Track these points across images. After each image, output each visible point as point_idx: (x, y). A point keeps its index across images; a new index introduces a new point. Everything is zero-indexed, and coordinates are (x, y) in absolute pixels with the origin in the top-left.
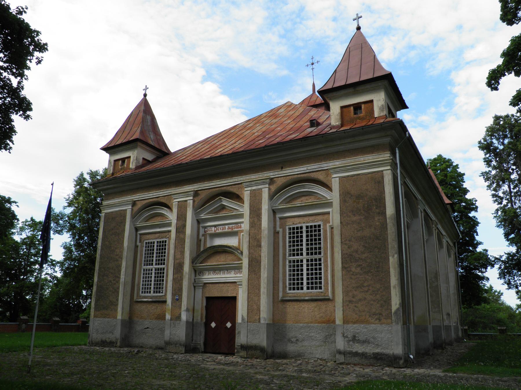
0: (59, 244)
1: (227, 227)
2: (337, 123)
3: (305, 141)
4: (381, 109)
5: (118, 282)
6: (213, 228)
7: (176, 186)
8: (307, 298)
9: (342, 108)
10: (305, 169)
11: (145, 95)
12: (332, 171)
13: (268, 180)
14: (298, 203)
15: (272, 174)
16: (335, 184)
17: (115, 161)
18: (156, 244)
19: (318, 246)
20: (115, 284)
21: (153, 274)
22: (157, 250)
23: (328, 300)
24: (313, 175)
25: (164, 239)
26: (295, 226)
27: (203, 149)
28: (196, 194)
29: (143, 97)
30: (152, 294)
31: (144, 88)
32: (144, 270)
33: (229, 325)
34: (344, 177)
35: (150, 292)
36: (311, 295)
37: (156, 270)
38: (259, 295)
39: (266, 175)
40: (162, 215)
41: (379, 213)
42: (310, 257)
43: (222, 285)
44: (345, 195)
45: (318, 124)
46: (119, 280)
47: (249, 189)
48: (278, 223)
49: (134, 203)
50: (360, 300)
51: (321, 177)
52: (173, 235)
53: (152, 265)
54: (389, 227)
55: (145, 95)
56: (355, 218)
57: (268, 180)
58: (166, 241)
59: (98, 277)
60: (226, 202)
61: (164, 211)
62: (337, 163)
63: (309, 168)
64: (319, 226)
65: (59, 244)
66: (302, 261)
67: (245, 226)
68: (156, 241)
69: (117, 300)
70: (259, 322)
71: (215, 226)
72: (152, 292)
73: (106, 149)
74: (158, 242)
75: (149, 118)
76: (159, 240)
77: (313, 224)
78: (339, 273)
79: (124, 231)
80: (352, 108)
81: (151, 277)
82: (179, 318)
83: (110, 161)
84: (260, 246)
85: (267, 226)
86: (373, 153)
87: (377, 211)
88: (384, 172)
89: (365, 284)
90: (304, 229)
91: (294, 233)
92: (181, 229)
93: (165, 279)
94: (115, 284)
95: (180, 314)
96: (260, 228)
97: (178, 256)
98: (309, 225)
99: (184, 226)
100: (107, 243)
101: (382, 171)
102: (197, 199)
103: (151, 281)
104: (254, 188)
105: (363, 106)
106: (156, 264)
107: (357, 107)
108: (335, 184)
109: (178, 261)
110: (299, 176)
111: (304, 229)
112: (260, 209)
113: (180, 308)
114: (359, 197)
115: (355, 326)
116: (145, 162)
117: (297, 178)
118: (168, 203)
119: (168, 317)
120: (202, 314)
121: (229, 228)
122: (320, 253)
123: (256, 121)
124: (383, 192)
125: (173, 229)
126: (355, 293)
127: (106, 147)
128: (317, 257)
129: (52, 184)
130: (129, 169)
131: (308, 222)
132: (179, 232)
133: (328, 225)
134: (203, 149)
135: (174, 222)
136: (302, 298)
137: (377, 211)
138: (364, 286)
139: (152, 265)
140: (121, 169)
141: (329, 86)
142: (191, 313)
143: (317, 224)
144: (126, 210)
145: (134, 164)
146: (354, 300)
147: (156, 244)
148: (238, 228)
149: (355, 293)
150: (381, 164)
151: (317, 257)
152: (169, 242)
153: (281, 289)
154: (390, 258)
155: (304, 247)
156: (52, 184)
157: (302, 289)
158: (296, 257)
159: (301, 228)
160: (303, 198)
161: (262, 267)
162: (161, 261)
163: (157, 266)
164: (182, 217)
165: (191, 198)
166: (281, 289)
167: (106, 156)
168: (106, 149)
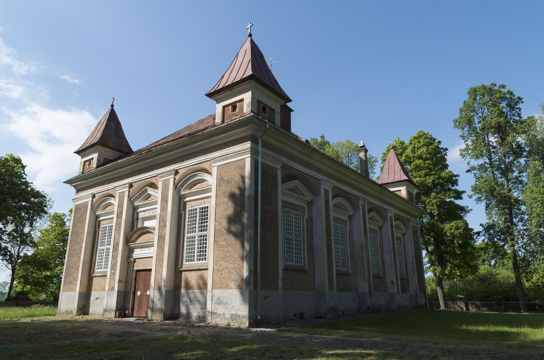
4: (248, 107)
5: (79, 261)
11: (112, 106)
12: (212, 161)
13: (173, 172)
14: (194, 189)
15: (176, 166)
16: (214, 171)
18: (198, 210)
21: (196, 241)
26: (192, 208)
28: (131, 186)
32: (187, 238)
36: (198, 265)
37: (199, 237)
38: (162, 267)
40: (203, 181)
42: (201, 233)
43: (145, 259)
44: (220, 180)
47: (162, 179)
50: (224, 269)
52: (115, 220)
54: (246, 206)
55: (112, 106)
57: (173, 172)
61: (206, 176)
71: (144, 211)
73: (78, 152)
75: (113, 125)
79: (86, 218)
82: (113, 289)
95: (114, 285)
102: (177, 177)
107: (234, 106)
108: (214, 171)
112: (167, 196)
115: (219, 291)
118: (209, 170)
119: (107, 288)
121: (152, 212)
126: (221, 262)
131: (200, 205)
139: (195, 232)
143: (206, 206)
145: (96, 164)
146: (220, 269)
149: (221, 262)
154: (245, 232)
158: (203, 232)
160: (199, 185)
162: (204, 228)
163: (201, 233)
167: (78, 160)
168: (78, 152)
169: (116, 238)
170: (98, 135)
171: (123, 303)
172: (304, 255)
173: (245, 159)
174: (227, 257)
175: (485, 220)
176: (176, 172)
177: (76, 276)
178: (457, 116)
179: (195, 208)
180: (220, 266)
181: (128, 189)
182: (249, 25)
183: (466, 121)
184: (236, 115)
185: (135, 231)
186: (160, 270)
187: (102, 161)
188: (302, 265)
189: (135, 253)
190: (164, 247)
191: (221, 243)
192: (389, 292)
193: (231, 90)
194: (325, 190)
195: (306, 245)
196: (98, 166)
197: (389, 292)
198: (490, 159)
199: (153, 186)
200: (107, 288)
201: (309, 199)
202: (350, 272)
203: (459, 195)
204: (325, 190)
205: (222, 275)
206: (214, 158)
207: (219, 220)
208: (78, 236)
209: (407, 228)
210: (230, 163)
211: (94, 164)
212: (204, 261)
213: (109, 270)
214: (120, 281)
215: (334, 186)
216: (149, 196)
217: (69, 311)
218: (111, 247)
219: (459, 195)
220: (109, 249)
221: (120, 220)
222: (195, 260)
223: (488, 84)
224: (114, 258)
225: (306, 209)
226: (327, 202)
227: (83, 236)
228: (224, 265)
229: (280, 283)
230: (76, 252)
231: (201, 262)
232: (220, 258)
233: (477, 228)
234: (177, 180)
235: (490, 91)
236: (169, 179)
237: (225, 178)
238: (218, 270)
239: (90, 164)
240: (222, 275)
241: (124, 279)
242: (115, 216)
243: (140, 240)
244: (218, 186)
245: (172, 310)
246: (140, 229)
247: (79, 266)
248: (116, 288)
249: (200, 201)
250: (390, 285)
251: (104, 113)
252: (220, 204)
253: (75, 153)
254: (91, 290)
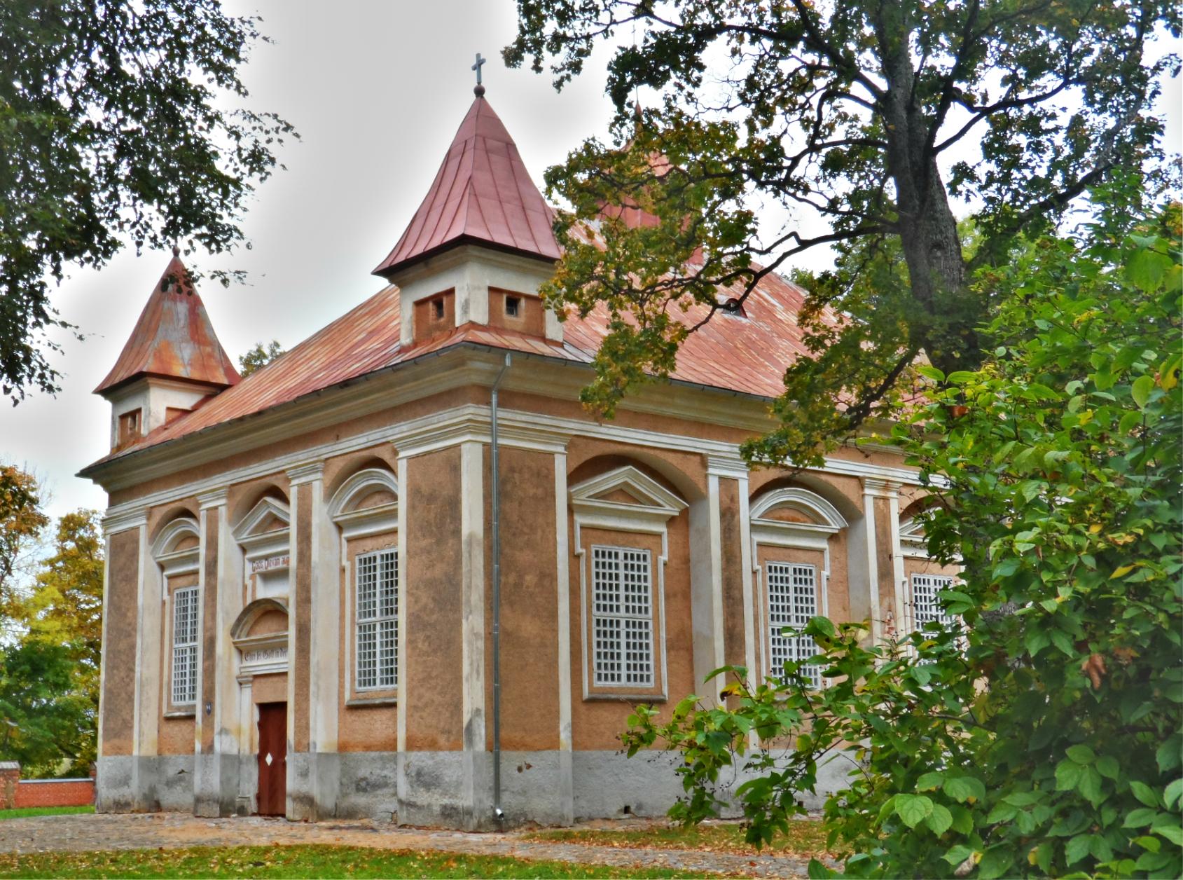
6: (264, 563)
7: (205, 477)
10: (364, 440)
11: (479, 92)
18: (378, 561)
26: (367, 556)
31: (474, 62)
34: (417, 456)
49: (149, 513)
55: (479, 92)
59: (107, 673)
62: (301, 457)
63: (371, 438)
69: (132, 717)
83: (113, 417)
86: (450, 406)
89: (434, 674)
97: (209, 624)
107: (440, 302)
113: (213, 729)
116: (176, 414)
119: (198, 747)
120: (252, 740)
127: (387, 265)
136: (613, 696)
138: (431, 678)
144: (138, 528)
149: (422, 690)
154: (464, 621)
165: (223, 501)
172: (658, 661)
173: (458, 445)
177: (128, 717)
179: (371, 554)
194: (723, 480)
195: (663, 634)
201: (671, 510)
202: (665, 690)
204: (723, 480)
210: (430, 452)
213: (198, 702)
217: (123, 800)
218: (199, 644)
220: (194, 650)
222: (378, 681)
225: (665, 539)
226: (729, 514)
228: (428, 696)
229: (565, 736)
236: (309, 483)
242: (201, 566)
247: (133, 693)
249: (381, 541)
253: (78, 475)
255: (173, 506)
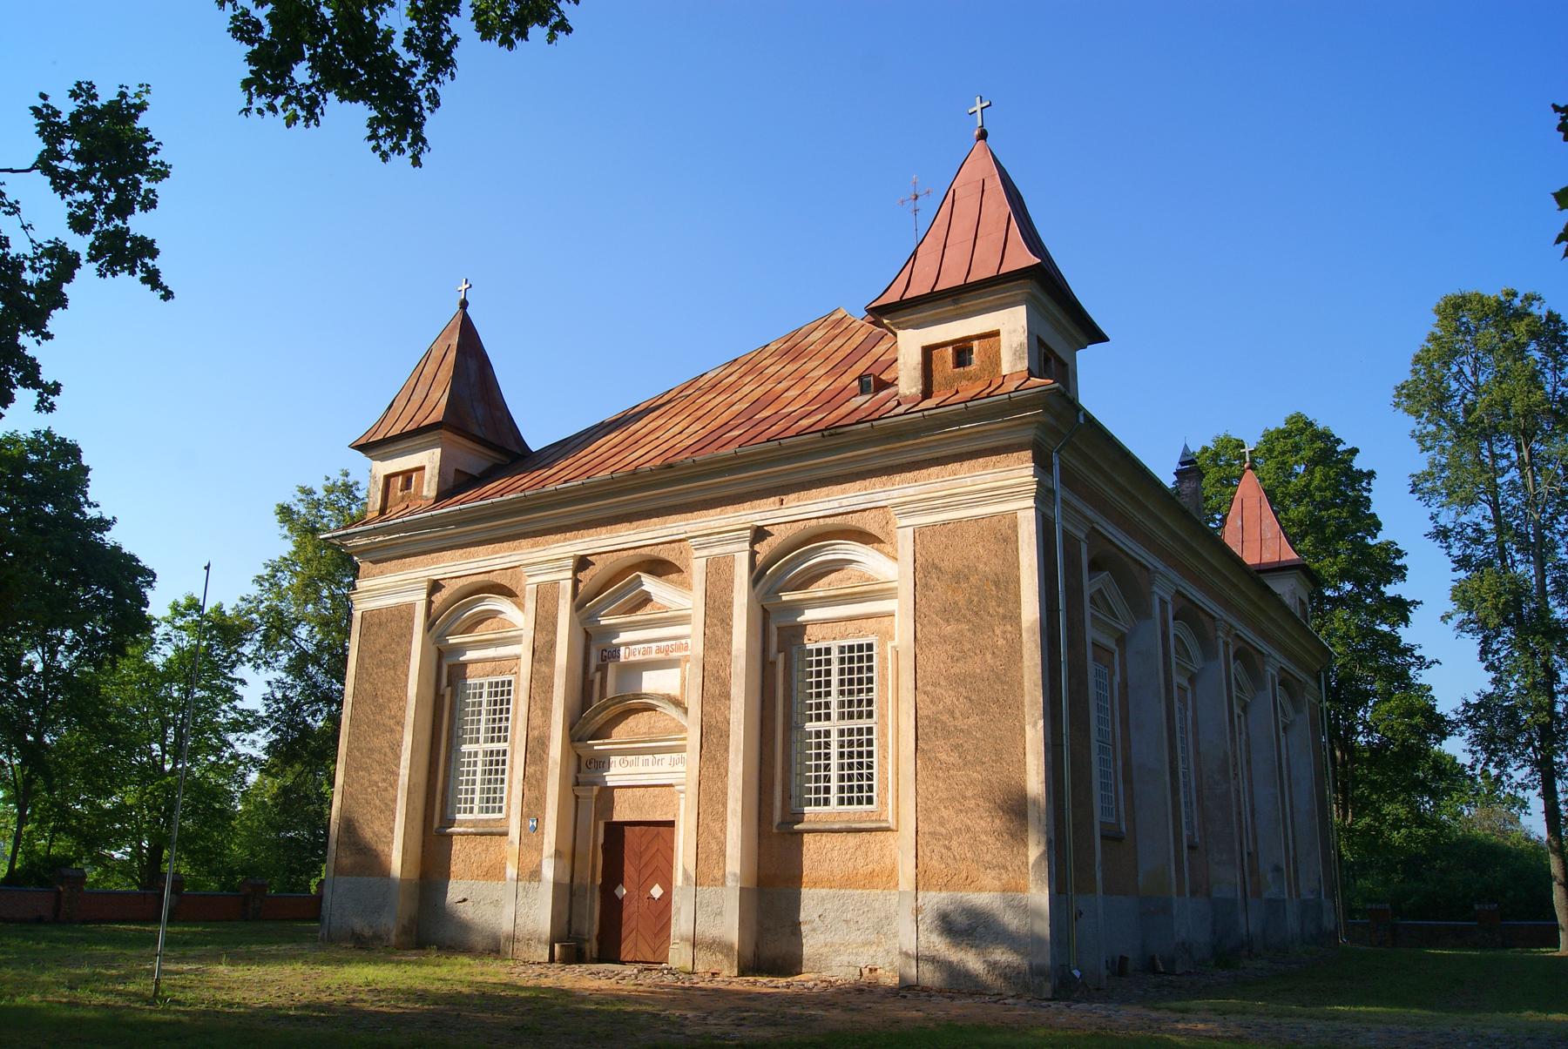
0: (256, 685)
1: (654, 645)
2: (914, 390)
3: (833, 436)
4: (1016, 354)
5: (394, 785)
8: (837, 826)
9: (928, 351)
11: (464, 304)
17: (388, 478)
18: (486, 690)
19: (863, 696)
20: (386, 790)
22: (489, 703)
23: (887, 829)
24: (854, 521)
25: (506, 678)
27: (604, 449)
28: (582, 563)
29: (457, 308)
30: (476, 815)
33: (657, 891)
35: (471, 811)
39: (743, 519)
40: (492, 614)
41: (1004, 617)
42: (847, 724)
44: (925, 572)
45: (882, 385)
46: (396, 781)
47: (705, 552)
48: (774, 640)
50: (958, 831)
51: (870, 524)
53: (477, 741)
55: (464, 304)
56: (949, 630)
58: (510, 683)
60: (649, 584)
62: (911, 491)
64: (870, 647)
65: (256, 685)
66: (828, 734)
67: (696, 646)
68: (486, 681)
69: (392, 831)
70: (724, 884)
72: (476, 809)
74: (490, 685)
75: (472, 364)
76: (494, 679)
77: (855, 642)
78: (908, 768)
79: (408, 655)
80: (950, 349)
81: (475, 773)
82: (535, 875)
84: (727, 696)
85: (744, 647)
87: (1001, 610)
88: (1019, 514)
90: (835, 655)
91: (851, 660)
92: (542, 653)
93: (506, 777)
94: (386, 790)
95: (540, 865)
96: (729, 653)
98: (846, 643)
99: (552, 645)
100: (367, 686)
101: (1014, 512)
102: (764, 549)
103: (474, 783)
104: (717, 551)
105: (976, 343)
106: (486, 741)
107: (962, 351)
109: (536, 733)
110: (830, 521)
111: (835, 655)
112: (729, 605)
114: (958, 577)
117: (819, 526)
119: (511, 871)
121: (659, 650)
122: (870, 714)
123: (749, 366)
124: (1016, 566)
125: (523, 650)
126: (945, 813)
128: (864, 723)
129: (207, 568)
130: (422, 497)
131: (843, 637)
132: (540, 661)
133: (890, 645)
134: (604, 449)
135: (528, 635)
137: (1001, 610)
139: (477, 741)
140: (403, 498)
141: (893, 297)
142: (567, 862)
143: (864, 641)
145: (434, 486)
147: (486, 690)
148: (679, 649)
149: (945, 813)
150: (1013, 493)
151: (864, 723)
152: (518, 683)
153: (778, 803)
154: (1028, 728)
155: (834, 699)
156: (207, 568)
157: (827, 802)
158: (856, 721)
159: (828, 651)
161: (731, 749)
163: (847, 724)
164: (545, 623)
166: (778, 803)
169: (536, 722)
170: (434, 396)
171: (566, 917)
172: (1117, 794)
174: (965, 798)
175: (1479, 682)
176: (759, 534)
178: (1404, 375)
180: (942, 824)
181: (569, 574)
182: (978, 108)
183: (1426, 396)
184: (973, 378)
185: (600, 699)
186: (716, 827)
187: (451, 478)
188: (1113, 820)
189: (613, 770)
190: (726, 759)
191: (943, 756)
192: (1265, 895)
193: (955, 302)
196: (444, 495)
197: (1265, 895)
198: (1495, 507)
199: (660, 567)
200: (511, 871)
203: (1401, 609)
205: (949, 849)
206: (905, 503)
207: (929, 688)
208: (382, 708)
209: (1298, 710)
211: (429, 489)
212: (865, 807)
214: (558, 854)
215: (1177, 592)
216: (646, 599)
219: (1401, 609)
221: (544, 669)
223: (1493, 291)
224: (534, 782)
227: (403, 709)
230: (376, 756)
231: (855, 807)
232: (941, 800)
233: (1447, 704)
234: (759, 558)
235: (1505, 313)
237: (945, 565)
238: (932, 834)
239: (407, 485)
240: (949, 849)
241: (567, 848)
243: (621, 732)
244: (921, 585)
245: (757, 946)
246: (622, 699)
247: (395, 801)
248: (548, 872)
249: (851, 626)
250: (1269, 877)
251: (430, 328)
252: (931, 642)
254: (447, 876)
255: (474, 579)
